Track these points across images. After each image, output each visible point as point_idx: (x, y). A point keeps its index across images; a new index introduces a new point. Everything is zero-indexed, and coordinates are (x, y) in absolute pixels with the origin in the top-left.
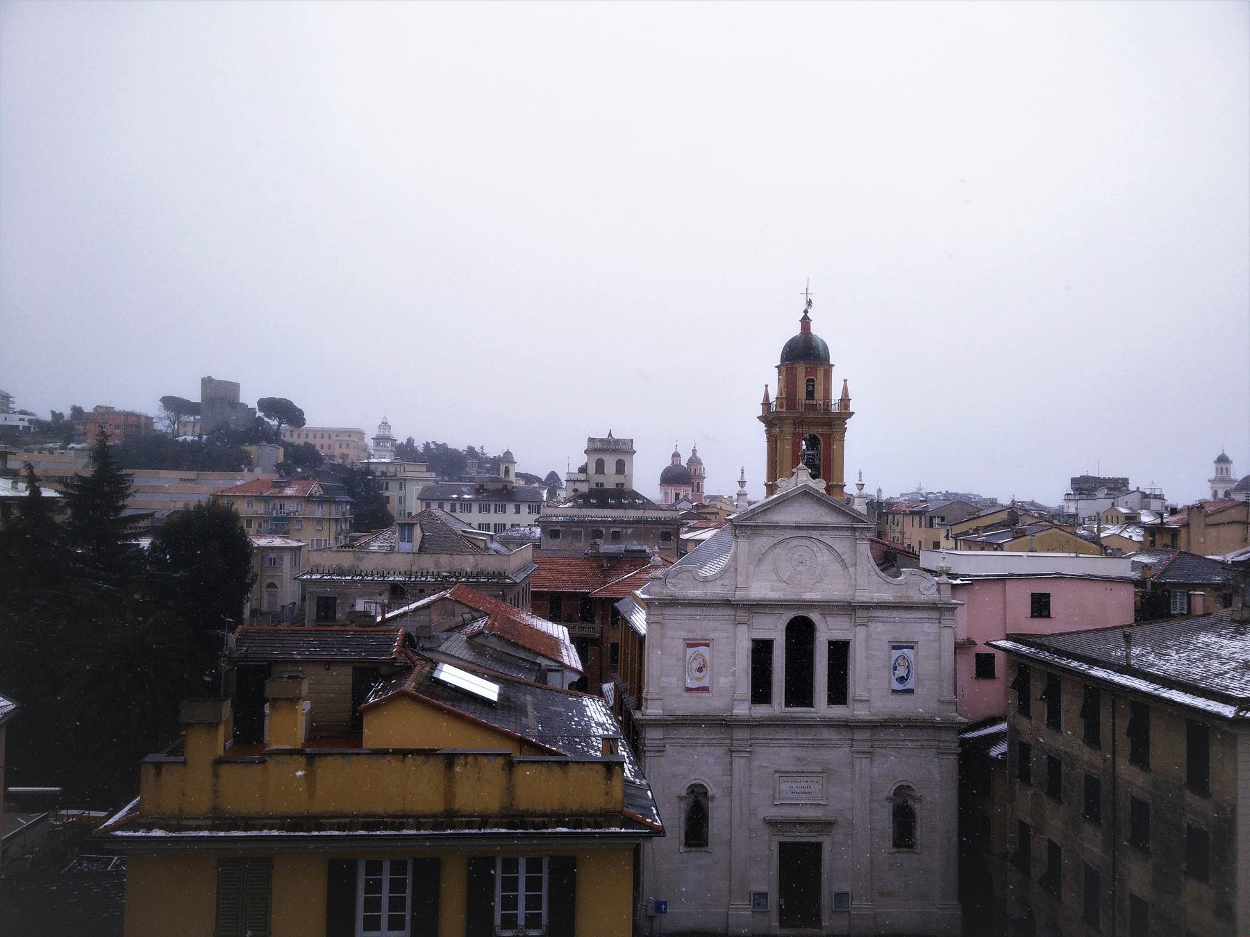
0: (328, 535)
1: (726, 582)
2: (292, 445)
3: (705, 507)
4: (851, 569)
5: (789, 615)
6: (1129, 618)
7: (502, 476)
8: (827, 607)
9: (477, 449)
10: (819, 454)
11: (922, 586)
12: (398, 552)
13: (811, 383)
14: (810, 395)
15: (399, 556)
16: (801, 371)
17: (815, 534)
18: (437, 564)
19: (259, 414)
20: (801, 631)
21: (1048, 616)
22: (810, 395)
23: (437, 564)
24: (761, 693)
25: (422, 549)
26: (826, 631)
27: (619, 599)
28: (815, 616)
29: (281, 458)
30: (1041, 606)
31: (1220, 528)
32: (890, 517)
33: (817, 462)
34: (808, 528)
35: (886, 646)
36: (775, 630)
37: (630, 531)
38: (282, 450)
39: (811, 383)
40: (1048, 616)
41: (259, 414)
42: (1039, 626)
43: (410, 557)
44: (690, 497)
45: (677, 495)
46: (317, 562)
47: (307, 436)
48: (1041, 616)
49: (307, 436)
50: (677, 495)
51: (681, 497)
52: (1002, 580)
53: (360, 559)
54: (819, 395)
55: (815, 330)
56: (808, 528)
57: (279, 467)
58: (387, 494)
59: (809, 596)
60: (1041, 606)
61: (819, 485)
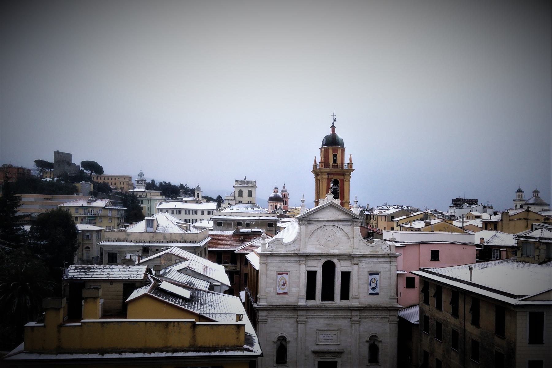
1: (296, 245)
2: (97, 183)
5: (324, 260)
8: (341, 257)
9: (185, 185)
13: (335, 156)
14: (335, 161)
17: (336, 224)
19: (82, 168)
20: (329, 268)
22: (335, 161)
26: (340, 267)
28: (335, 261)
34: (332, 221)
38: (92, 185)
39: (335, 156)
41: (82, 168)
44: (282, 208)
45: (276, 207)
51: (278, 207)
52: (418, 244)
56: (332, 221)
58: (142, 206)
59: (332, 252)
61: (338, 202)
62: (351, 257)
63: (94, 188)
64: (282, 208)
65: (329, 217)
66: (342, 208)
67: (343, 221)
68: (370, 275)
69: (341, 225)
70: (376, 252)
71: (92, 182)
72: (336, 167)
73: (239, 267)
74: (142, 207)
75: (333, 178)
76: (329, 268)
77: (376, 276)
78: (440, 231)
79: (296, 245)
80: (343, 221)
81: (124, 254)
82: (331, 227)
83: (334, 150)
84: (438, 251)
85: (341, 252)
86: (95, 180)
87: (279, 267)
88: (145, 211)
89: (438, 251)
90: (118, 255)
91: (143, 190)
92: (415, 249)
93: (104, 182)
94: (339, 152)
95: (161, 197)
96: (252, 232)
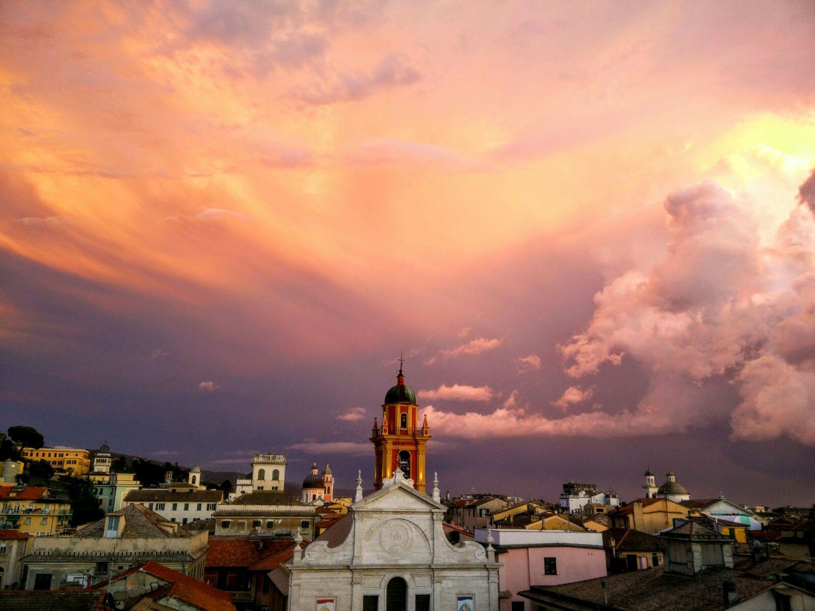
0: (51, 526)
1: (347, 553)
2: (31, 461)
3: (332, 504)
4: (431, 542)
5: (389, 576)
6: (604, 573)
7: (190, 482)
8: (414, 568)
9: (173, 463)
10: (409, 462)
11: (476, 553)
12: (105, 538)
13: (404, 417)
14: (404, 424)
15: (106, 540)
16: (398, 407)
17: (407, 517)
18: (135, 547)
19: (9, 438)
20: (397, 588)
21: (555, 574)
22: (404, 424)
23: (135, 547)
24: (102, 490)
25: (124, 536)
26: (416, 586)
27: (270, 571)
28: (407, 577)
29: (21, 471)
30: (551, 566)
31: (674, 511)
32: (455, 510)
33: (408, 469)
34: (402, 512)
35: (454, 597)
36: (378, 587)
37: (280, 521)
38: (22, 464)
39: (404, 417)
40: (555, 574)
41: (9, 438)
42: (551, 581)
43: (114, 541)
44: (323, 498)
45: (314, 496)
46: (41, 546)
47: (44, 455)
48: (551, 573)
49: (44, 455)
50: (314, 496)
51: (317, 497)
52: (527, 547)
53: (74, 544)
54: (410, 424)
55: (406, 382)
56: (402, 512)
57: (18, 477)
58: (100, 497)
59: (402, 562)
60: (551, 566)
61: (410, 483)
62: (431, 569)
63: (25, 468)
64: (323, 498)
65: (397, 507)
66: (415, 492)
67: (419, 513)
68: (460, 599)
69: (415, 518)
70: (467, 561)
71: (23, 460)
72: (405, 433)
73: (253, 592)
74: (101, 500)
75: (402, 448)
76: (397, 588)
77: (467, 601)
78: (553, 529)
79: (347, 553)
80: (419, 513)
81: (64, 576)
82: (400, 523)
83: (402, 409)
84: (554, 559)
85: (415, 562)
86: (29, 457)
87: (320, 591)
88: (104, 506)
89: (554, 559)
90: (53, 577)
91: (68, 499)
92: (524, 551)
93: (42, 460)
94: (410, 411)
95: (134, 482)
96: (436, 388)
